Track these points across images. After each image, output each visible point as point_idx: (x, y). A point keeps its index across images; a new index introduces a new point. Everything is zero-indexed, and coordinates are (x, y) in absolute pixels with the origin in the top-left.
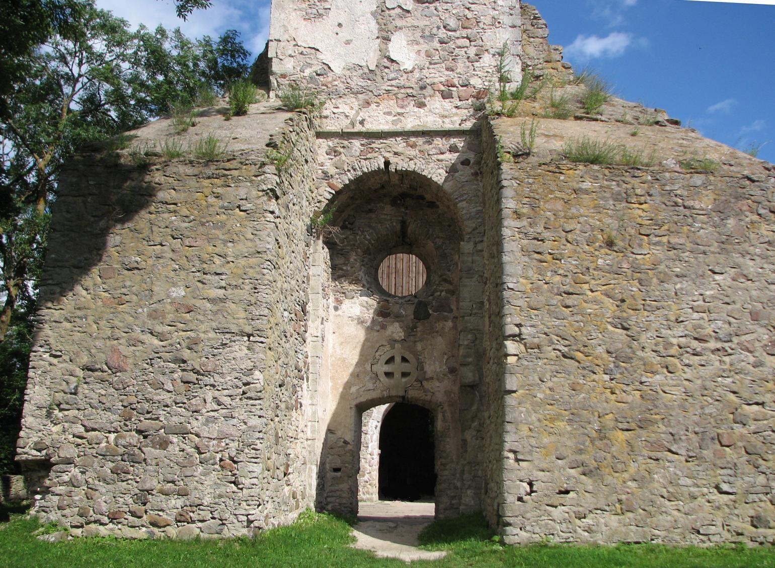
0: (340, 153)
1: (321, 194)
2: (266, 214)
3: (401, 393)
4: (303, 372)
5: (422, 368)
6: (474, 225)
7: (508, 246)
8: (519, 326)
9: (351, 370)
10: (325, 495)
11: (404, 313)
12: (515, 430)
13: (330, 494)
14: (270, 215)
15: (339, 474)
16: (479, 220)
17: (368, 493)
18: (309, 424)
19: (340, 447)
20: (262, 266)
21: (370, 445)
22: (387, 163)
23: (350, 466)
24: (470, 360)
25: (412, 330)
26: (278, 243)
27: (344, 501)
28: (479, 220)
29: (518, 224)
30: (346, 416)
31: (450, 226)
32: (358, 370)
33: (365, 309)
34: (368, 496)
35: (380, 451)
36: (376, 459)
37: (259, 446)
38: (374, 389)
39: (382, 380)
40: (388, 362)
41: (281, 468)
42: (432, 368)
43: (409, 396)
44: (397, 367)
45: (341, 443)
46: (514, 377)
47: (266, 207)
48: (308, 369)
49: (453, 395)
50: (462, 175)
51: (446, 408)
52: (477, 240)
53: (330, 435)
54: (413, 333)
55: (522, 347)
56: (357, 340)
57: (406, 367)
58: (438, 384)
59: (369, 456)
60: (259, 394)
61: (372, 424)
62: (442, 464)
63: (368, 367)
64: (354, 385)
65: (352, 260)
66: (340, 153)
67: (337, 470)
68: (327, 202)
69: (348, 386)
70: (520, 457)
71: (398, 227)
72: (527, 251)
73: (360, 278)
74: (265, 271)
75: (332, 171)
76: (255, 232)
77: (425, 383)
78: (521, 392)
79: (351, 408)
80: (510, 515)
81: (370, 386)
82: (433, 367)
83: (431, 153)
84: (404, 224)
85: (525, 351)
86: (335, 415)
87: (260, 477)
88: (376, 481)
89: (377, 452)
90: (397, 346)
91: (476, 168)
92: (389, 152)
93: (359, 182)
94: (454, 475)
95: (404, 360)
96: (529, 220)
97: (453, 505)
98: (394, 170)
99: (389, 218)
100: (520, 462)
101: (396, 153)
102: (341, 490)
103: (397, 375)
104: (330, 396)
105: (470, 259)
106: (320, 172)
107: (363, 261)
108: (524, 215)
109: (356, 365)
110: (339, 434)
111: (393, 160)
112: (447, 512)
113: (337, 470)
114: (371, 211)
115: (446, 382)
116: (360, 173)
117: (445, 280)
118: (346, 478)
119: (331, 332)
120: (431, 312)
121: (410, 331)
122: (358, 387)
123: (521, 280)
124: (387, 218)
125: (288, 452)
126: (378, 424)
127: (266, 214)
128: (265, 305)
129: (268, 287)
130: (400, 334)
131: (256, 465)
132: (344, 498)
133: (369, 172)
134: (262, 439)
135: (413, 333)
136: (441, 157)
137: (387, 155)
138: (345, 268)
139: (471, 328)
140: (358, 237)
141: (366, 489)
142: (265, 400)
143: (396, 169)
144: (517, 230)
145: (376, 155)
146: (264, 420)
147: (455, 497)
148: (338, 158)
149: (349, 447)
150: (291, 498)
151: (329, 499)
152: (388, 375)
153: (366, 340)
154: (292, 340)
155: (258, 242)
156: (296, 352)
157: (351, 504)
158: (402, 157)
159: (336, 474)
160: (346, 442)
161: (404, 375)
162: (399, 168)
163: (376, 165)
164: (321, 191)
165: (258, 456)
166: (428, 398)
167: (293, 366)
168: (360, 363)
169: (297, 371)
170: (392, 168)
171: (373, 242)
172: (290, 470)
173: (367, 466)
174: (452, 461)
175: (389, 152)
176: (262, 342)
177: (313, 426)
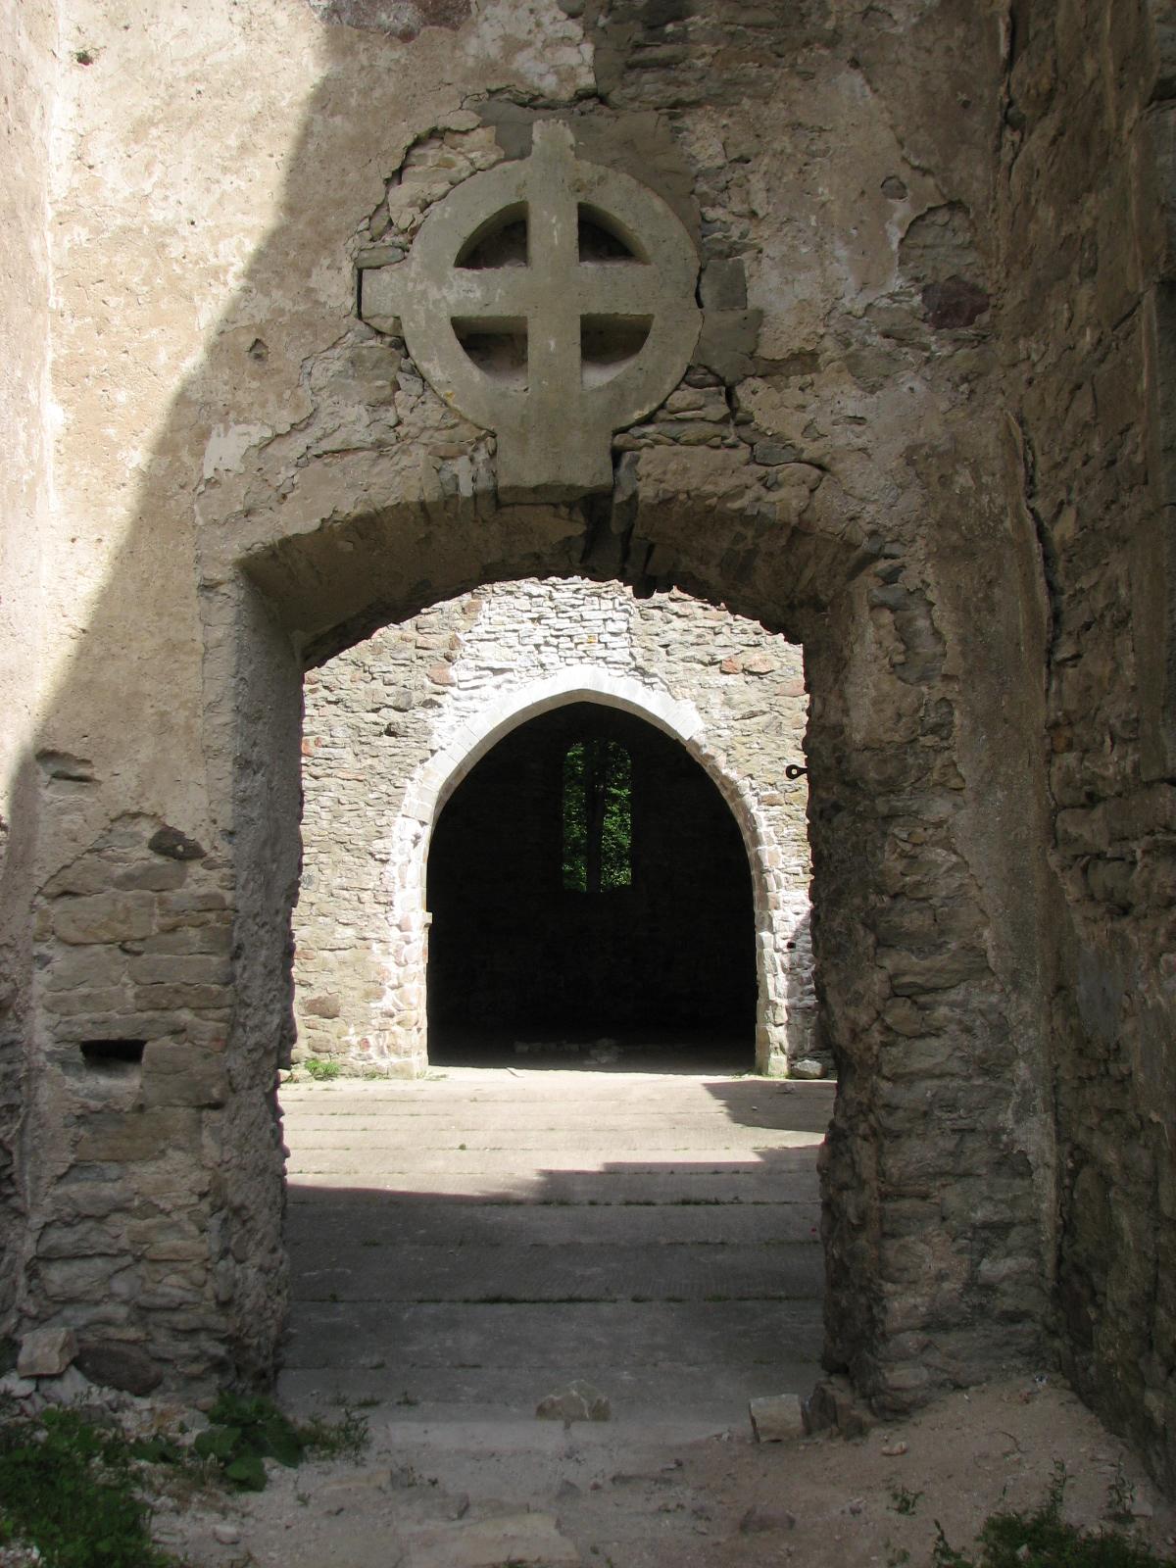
3: (586, 470)
5: (735, 292)
9: (208, 313)
10: (28, 1248)
15: (123, 1085)
17: (394, 1049)
19: (128, 881)
21: (397, 899)
23: (209, 1026)
25: (653, 27)
27: (172, 1286)
30: (173, 647)
32: (261, 309)
34: (394, 1059)
35: (428, 918)
36: (420, 940)
38: (379, 446)
39: (435, 371)
40: (478, 253)
42: (806, 286)
43: (647, 492)
44: (550, 288)
45: (140, 855)
49: (964, 479)
51: (919, 569)
53: (53, 795)
54: (663, 52)
56: (253, 101)
57: (611, 289)
58: (852, 402)
59: (395, 933)
62: (897, 991)
63: (334, 287)
64: (231, 414)
67: (111, 1053)
69: (191, 419)
77: (755, 396)
79: (208, 587)
81: (353, 421)
82: (815, 276)
86: (98, 642)
88: (419, 1013)
89: (419, 918)
94: (990, 1067)
95: (599, 238)
97: (989, 1288)
102: (149, 1209)
103: (552, 342)
104: (53, 503)
109: (251, 274)
110: (120, 782)
112: (952, 1341)
113: (111, 1053)
115: (911, 383)
118: (183, 1115)
119: (67, 48)
122: (258, 433)
130: (569, 57)
132: (172, 1261)
135: (663, 52)
141: (389, 1039)
147: (1001, 1228)
149: (200, 882)
151: (56, 1276)
152: (488, 342)
153: (324, 99)
157: (224, 1305)
159: (103, 1082)
160: (172, 846)
161: (606, 339)
166: (786, 501)
168: (279, 260)
173: (389, 963)
174: (976, 968)
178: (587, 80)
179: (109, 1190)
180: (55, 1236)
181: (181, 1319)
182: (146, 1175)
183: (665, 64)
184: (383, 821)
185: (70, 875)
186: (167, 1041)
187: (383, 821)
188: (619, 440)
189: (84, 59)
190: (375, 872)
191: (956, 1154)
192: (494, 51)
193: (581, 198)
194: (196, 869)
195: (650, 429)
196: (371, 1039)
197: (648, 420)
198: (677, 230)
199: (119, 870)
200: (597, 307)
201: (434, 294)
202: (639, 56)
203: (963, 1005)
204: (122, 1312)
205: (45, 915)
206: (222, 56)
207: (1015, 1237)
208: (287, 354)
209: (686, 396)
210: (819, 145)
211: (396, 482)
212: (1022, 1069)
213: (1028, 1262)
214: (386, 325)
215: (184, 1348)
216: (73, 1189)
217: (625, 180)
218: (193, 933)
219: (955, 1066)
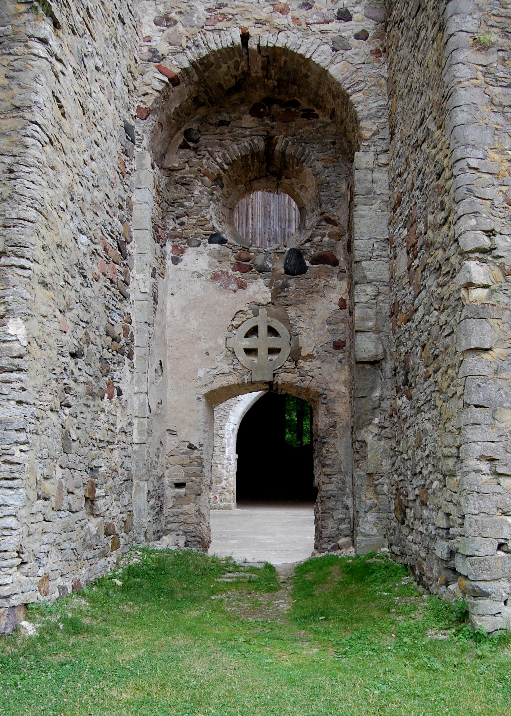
0: (176, 22)
1: (149, 82)
2: (30, 43)
3: (268, 378)
4: (122, 343)
6: (375, 128)
7: (464, 96)
8: (490, 233)
11: (270, 266)
12: (490, 420)
13: (171, 519)
14: (39, 45)
15: (182, 491)
16: (382, 121)
17: (225, 500)
18: (136, 421)
19: (183, 453)
20: (23, 132)
22: (245, 37)
24: (371, 324)
26: (61, 107)
28: (382, 121)
29: (482, 58)
31: (334, 143)
33: (215, 261)
34: (225, 503)
35: (237, 456)
37: (18, 456)
41: (77, 491)
43: (280, 382)
45: (186, 449)
46: (486, 325)
47: (30, 31)
48: (132, 341)
50: (356, 54)
52: (379, 149)
55: (497, 271)
57: (274, 342)
59: (226, 462)
60: (17, 361)
61: (229, 427)
65: (196, 192)
66: (176, 22)
67: (179, 485)
68: (157, 94)
70: (501, 470)
71: (262, 145)
72: (501, 105)
73: (208, 217)
74: (29, 141)
75: (164, 48)
76: (12, 74)
78: (497, 351)
79: (199, 399)
80: (485, 577)
81: (226, 368)
83: (311, 21)
84: (270, 141)
85: (502, 279)
87: (23, 513)
89: (234, 456)
90: (263, 312)
91: (377, 44)
92: (249, 19)
93: (203, 66)
95: (272, 331)
96: (501, 54)
97: (342, 531)
98: (255, 47)
99: (248, 133)
100: (501, 479)
101: (258, 22)
102: (187, 514)
103: (263, 352)
105: (369, 177)
106: (145, 50)
107: (212, 194)
108: (493, 44)
111: (253, 31)
113: (179, 485)
114: (222, 123)
116: (204, 52)
117: (328, 220)
120: (308, 263)
121: (279, 292)
123: (491, 153)
124: (245, 135)
125: (95, 463)
126: (235, 426)
127: (30, 43)
128: (29, 202)
129: (34, 169)
130: (266, 295)
131: (11, 492)
133: (219, 51)
134: (25, 443)
135: (284, 294)
136: (325, 27)
137: (245, 24)
138: (187, 204)
139: (371, 277)
140: (204, 161)
141: (223, 497)
142: (32, 373)
143: (258, 45)
144: (480, 68)
145: (229, 24)
146: (29, 410)
147: (344, 519)
148: (172, 29)
150: (103, 536)
154: (97, 286)
155: (16, 90)
156: (108, 308)
158: (267, 27)
159: (177, 490)
161: (272, 351)
162: (263, 44)
163: (229, 38)
164: (147, 78)
165: (17, 475)
167: (102, 329)
169: (109, 339)
170: (252, 44)
171: (226, 167)
172: (99, 492)
175: (249, 19)
176: (23, 268)
177: (140, 424)
178: (270, 300)
179: (179, 510)
180: (169, 519)
181: (193, 534)
182: (186, 508)
183: (285, 297)
184: (222, 424)
185: (172, 452)
186: (190, 483)
187: (222, 424)
188: (275, 372)
189: (172, 294)
190: (219, 441)
191: (335, 505)
192: (252, 294)
193: (268, 324)
194: (196, 451)
195: (281, 370)
196: (218, 497)
197: (281, 368)
198: (286, 331)
199: (182, 451)
200: (271, 347)
201: (240, 343)
202: (279, 295)
203: (337, 478)
204: (182, 533)
205: (168, 460)
206: (199, 295)
207: (346, 521)
208: (212, 354)
209: (288, 363)
210: (314, 313)
211: (233, 380)
212: (347, 490)
213: (349, 525)
214: (231, 349)
215: (193, 539)
216: (173, 510)
217: (277, 321)
218: (196, 463)
219: (335, 489)
